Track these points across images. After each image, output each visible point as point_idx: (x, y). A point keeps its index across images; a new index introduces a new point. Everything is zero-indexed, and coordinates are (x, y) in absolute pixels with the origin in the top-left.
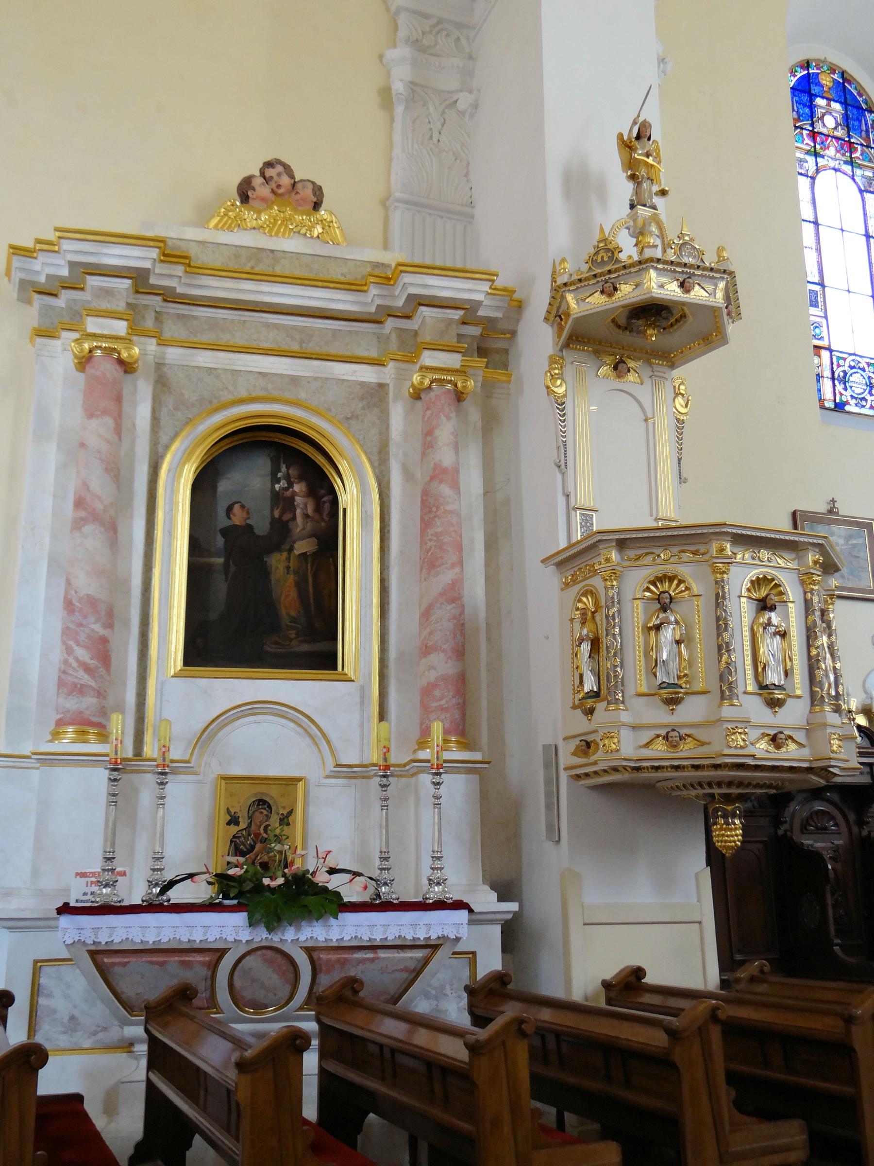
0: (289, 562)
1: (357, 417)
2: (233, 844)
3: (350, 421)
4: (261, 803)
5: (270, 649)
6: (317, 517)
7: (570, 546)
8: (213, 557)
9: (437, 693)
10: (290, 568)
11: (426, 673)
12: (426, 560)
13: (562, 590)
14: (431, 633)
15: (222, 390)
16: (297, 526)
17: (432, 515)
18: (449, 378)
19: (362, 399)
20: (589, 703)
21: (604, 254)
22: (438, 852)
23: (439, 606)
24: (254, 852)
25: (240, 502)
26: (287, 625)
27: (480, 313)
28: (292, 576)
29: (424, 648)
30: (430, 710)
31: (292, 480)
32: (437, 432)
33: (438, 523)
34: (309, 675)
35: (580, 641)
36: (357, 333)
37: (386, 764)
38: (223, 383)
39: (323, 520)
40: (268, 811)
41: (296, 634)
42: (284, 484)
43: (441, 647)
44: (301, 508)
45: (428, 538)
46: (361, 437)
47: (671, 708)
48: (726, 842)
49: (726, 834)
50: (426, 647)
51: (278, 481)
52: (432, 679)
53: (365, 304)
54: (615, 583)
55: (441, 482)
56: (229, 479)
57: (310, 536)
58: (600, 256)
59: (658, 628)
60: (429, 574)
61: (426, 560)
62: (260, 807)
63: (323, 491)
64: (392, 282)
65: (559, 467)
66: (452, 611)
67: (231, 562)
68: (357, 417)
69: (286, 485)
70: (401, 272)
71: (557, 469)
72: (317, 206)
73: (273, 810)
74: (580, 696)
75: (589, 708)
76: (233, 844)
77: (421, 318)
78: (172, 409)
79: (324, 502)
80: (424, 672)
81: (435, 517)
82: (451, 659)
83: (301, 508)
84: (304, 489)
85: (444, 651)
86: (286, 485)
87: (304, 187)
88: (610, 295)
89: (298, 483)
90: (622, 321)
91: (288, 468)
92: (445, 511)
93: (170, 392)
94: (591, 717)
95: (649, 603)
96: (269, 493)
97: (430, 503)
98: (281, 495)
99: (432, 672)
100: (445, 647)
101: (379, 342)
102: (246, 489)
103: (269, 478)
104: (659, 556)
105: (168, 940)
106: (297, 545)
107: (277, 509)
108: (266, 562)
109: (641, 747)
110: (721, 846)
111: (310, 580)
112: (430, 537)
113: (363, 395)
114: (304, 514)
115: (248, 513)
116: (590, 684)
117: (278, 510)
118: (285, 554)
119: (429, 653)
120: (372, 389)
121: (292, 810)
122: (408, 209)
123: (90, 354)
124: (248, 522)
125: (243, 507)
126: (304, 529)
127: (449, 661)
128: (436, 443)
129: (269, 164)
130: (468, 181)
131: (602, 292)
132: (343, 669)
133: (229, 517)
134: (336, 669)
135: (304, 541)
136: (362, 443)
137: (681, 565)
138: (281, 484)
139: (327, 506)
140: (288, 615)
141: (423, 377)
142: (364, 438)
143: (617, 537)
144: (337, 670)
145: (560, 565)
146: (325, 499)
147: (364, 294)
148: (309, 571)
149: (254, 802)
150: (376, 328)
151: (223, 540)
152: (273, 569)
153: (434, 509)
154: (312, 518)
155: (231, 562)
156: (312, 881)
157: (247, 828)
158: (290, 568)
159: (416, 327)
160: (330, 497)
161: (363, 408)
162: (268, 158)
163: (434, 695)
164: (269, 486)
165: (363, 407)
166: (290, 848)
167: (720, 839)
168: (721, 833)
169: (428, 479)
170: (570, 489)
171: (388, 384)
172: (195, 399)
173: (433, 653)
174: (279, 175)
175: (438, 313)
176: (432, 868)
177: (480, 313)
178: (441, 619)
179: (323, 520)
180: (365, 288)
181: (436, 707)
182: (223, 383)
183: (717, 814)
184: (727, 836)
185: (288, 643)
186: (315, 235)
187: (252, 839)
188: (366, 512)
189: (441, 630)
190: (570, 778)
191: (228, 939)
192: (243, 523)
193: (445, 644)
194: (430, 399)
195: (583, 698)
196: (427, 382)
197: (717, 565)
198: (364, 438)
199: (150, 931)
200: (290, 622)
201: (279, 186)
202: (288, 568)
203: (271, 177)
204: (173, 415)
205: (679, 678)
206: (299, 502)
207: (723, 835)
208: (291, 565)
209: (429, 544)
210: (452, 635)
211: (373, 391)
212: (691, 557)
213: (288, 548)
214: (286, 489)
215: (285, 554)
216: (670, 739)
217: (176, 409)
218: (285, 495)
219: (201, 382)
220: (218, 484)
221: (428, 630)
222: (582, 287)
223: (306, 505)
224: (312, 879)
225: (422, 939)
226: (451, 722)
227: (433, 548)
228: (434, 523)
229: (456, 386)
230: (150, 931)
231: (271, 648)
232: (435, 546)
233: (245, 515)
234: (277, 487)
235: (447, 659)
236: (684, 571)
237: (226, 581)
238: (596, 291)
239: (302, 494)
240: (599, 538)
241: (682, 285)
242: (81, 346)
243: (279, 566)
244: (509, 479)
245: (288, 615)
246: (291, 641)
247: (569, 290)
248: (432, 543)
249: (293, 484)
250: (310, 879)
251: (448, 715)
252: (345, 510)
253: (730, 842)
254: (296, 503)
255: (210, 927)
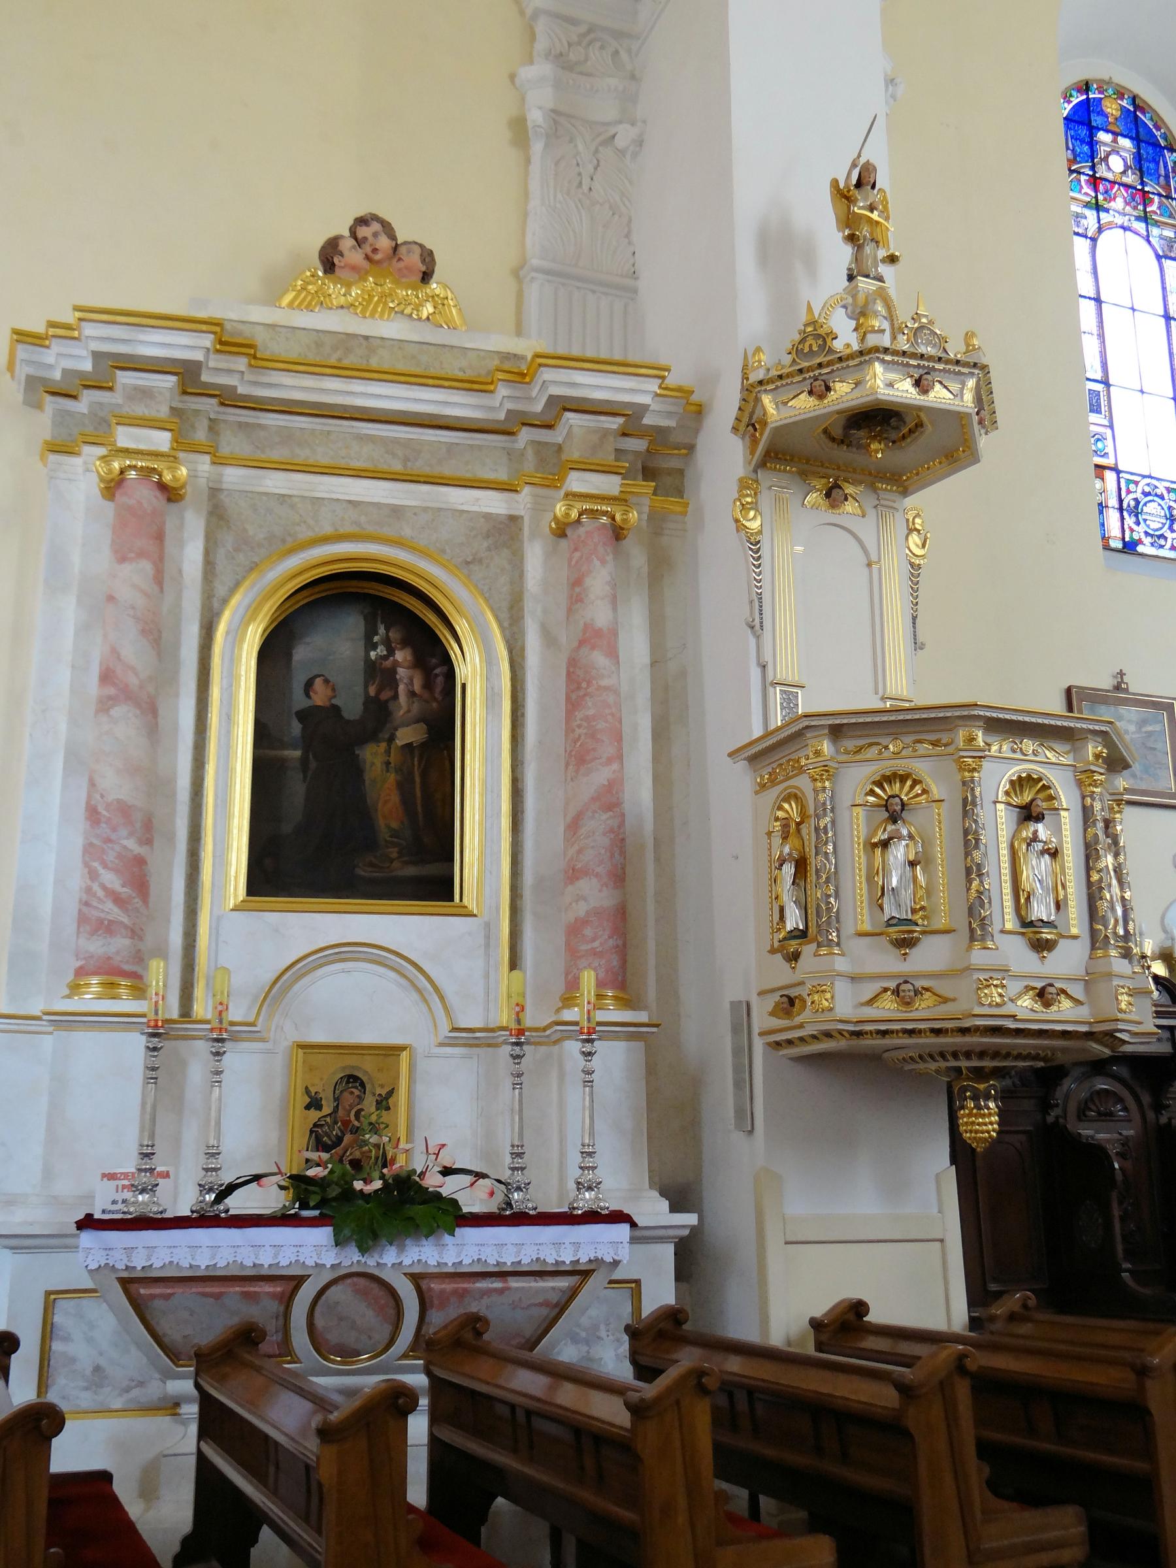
0: (389, 756)
1: (480, 561)
2: (314, 1134)
3: (471, 566)
4: (351, 1080)
5: (363, 873)
6: (426, 695)
7: (767, 734)
8: (287, 749)
9: (588, 932)
10: (390, 763)
11: (574, 904)
12: (573, 753)
13: (757, 793)
14: (580, 851)
15: (298, 525)
16: (400, 707)
17: (581, 693)
18: (604, 508)
19: (488, 536)
20: (793, 945)
21: (813, 342)
22: (589, 1145)
23: (591, 814)
24: (342, 1145)
25: (323, 676)
26: (386, 841)
27: (646, 421)
28: (393, 775)
29: (571, 871)
30: (579, 955)
31: (393, 645)
32: (588, 581)
33: (590, 704)
34: (416, 908)
35: (781, 862)
36: (480, 447)
37: (520, 1027)
38: (301, 516)
39: (435, 699)
40: (360, 1091)
41: (398, 853)
42: (382, 651)
43: (593, 871)
44: (406, 684)
45: (576, 723)
46: (486, 588)
47: (903, 952)
48: (977, 1132)
49: (977, 1121)
50: (573, 870)
51: (374, 647)
52: (582, 913)
53: (491, 409)
54: (827, 784)
55: (593, 648)
56: (308, 644)
57: (417, 721)
58: (807, 344)
59: (885, 844)
60: (577, 771)
61: (573, 753)
62: (350, 1085)
63: (434, 661)
64: (527, 379)
65: (752, 627)
66: (609, 822)
67: (311, 756)
68: (480, 561)
69: (385, 653)
70: (540, 365)
71: (749, 631)
72: (426, 277)
73: (367, 1089)
74: (781, 936)
75: (793, 952)
76: (314, 1134)
77: (567, 427)
78: (231, 550)
79: (437, 675)
80: (571, 904)
81: (585, 695)
82: (607, 887)
83: (406, 684)
84: (409, 658)
85: (597, 875)
86: (385, 653)
87: (409, 252)
88: (821, 397)
89: (402, 649)
90: (838, 432)
91: (387, 629)
92: (599, 688)
93: (229, 528)
94: (795, 964)
95: (874, 811)
96: (363, 663)
97: (579, 676)
98: (378, 665)
99: (582, 903)
100: (599, 870)
101: (510, 459)
102: (331, 657)
103: (362, 643)
104: (886, 748)
105: (226, 1264)
106: (399, 733)
107: (373, 685)
108: (359, 755)
109: (862, 1004)
110: (969, 1138)
111: (418, 779)
112: (578, 722)
113: (489, 531)
114: (409, 691)
115: (334, 690)
116: (793, 920)
117: (375, 686)
118: (384, 745)
119: (578, 879)
120: (501, 523)
121: (393, 1089)
122: (549, 281)
123: (121, 476)
124: (334, 701)
125: (327, 681)
126: (409, 711)
127: (605, 889)
128: (587, 596)
129: (362, 221)
130: (630, 243)
131: (811, 393)
132: (461, 900)
133: (308, 695)
134: (452, 899)
135: (409, 728)
136: (487, 595)
137: (917, 759)
138: (378, 650)
139: (440, 680)
140: (388, 826)
141: (570, 507)
142: (490, 589)
143: (830, 722)
144: (453, 901)
145: (753, 759)
146: (437, 671)
147: (490, 395)
148: (416, 768)
149: (342, 1078)
150: (506, 441)
151: (300, 726)
152: (368, 766)
153: (584, 685)
154: (420, 696)
155: (311, 756)
156: (420, 1185)
157: (332, 1113)
158: (390, 763)
159: (560, 440)
160: (444, 669)
161: (489, 549)
162: (360, 213)
163: (584, 935)
164: (362, 653)
165: (488, 547)
166: (390, 1141)
167: (969, 1128)
168: (971, 1120)
169: (575, 644)
170: (768, 657)
171: (522, 517)
172: (262, 536)
173: (582, 878)
174: (375, 235)
175: (589, 420)
176: (581, 1168)
177: (646, 421)
178: (594, 833)
179: (435, 699)
180: (492, 387)
181: (587, 950)
182: (301, 516)
183: (965, 1095)
184: (979, 1124)
185: (388, 865)
186: (424, 316)
187: (339, 1128)
188: (492, 688)
189: (593, 847)
190: (767, 1046)
191: (307, 1263)
192: (327, 704)
193: (599, 866)
194: (579, 536)
195: (785, 939)
196: (574, 514)
197: (965, 760)
198: (490, 589)
199: (202, 1252)
200: (391, 836)
201: (375, 250)
202: (388, 763)
203: (365, 239)
204: (233, 558)
205: (914, 911)
206: (403, 675)
207: (973, 1123)
208: (392, 760)
209: (578, 731)
210: (608, 854)
211: (501, 526)
212: (929, 749)
213: (387, 736)
214: (385, 658)
215: (384, 745)
216: (902, 994)
217: (237, 550)
218: (383, 666)
219: (270, 514)
220: (294, 651)
221: (576, 847)
222: (783, 385)
223: (411, 680)
224: (420, 1182)
225: (568, 1262)
226: (607, 971)
227: (583, 737)
228: (583, 703)
229: (613, 518)
230: (202, 1252)
231: (364, 871)
232: (586, 734)
233: (329, 693)
234: (373, 654)
235: (602, 886)
236: (920, 767)
237: (304, 781)
238: (803, 392)
239: (406, 664)
240: (807, 723)
241: (917, 383)
242: (108, 465)
243: (375, 761)
244: (684, 644)
245: (388, 826)
246: (392, 863)
247: (765, 391)
248: (581, 731)
249: (394, 651)
250: (417, 1182)
251: (603, 962)
252: (464, 686)
253: (982, 1132)
254: (398, 677)
255: (282, 1246)
